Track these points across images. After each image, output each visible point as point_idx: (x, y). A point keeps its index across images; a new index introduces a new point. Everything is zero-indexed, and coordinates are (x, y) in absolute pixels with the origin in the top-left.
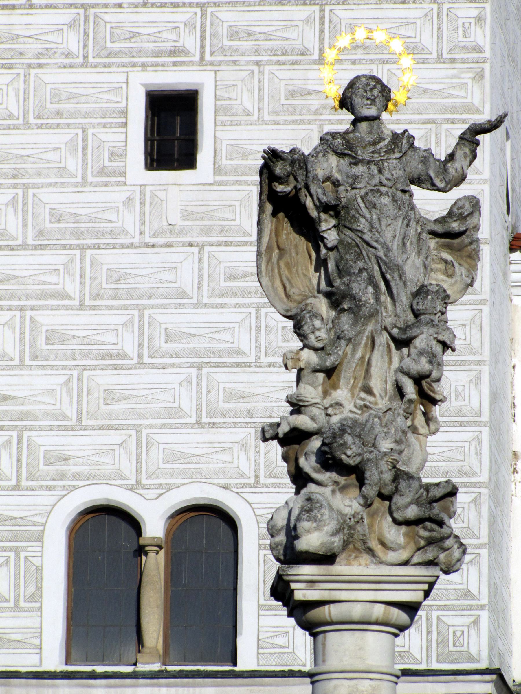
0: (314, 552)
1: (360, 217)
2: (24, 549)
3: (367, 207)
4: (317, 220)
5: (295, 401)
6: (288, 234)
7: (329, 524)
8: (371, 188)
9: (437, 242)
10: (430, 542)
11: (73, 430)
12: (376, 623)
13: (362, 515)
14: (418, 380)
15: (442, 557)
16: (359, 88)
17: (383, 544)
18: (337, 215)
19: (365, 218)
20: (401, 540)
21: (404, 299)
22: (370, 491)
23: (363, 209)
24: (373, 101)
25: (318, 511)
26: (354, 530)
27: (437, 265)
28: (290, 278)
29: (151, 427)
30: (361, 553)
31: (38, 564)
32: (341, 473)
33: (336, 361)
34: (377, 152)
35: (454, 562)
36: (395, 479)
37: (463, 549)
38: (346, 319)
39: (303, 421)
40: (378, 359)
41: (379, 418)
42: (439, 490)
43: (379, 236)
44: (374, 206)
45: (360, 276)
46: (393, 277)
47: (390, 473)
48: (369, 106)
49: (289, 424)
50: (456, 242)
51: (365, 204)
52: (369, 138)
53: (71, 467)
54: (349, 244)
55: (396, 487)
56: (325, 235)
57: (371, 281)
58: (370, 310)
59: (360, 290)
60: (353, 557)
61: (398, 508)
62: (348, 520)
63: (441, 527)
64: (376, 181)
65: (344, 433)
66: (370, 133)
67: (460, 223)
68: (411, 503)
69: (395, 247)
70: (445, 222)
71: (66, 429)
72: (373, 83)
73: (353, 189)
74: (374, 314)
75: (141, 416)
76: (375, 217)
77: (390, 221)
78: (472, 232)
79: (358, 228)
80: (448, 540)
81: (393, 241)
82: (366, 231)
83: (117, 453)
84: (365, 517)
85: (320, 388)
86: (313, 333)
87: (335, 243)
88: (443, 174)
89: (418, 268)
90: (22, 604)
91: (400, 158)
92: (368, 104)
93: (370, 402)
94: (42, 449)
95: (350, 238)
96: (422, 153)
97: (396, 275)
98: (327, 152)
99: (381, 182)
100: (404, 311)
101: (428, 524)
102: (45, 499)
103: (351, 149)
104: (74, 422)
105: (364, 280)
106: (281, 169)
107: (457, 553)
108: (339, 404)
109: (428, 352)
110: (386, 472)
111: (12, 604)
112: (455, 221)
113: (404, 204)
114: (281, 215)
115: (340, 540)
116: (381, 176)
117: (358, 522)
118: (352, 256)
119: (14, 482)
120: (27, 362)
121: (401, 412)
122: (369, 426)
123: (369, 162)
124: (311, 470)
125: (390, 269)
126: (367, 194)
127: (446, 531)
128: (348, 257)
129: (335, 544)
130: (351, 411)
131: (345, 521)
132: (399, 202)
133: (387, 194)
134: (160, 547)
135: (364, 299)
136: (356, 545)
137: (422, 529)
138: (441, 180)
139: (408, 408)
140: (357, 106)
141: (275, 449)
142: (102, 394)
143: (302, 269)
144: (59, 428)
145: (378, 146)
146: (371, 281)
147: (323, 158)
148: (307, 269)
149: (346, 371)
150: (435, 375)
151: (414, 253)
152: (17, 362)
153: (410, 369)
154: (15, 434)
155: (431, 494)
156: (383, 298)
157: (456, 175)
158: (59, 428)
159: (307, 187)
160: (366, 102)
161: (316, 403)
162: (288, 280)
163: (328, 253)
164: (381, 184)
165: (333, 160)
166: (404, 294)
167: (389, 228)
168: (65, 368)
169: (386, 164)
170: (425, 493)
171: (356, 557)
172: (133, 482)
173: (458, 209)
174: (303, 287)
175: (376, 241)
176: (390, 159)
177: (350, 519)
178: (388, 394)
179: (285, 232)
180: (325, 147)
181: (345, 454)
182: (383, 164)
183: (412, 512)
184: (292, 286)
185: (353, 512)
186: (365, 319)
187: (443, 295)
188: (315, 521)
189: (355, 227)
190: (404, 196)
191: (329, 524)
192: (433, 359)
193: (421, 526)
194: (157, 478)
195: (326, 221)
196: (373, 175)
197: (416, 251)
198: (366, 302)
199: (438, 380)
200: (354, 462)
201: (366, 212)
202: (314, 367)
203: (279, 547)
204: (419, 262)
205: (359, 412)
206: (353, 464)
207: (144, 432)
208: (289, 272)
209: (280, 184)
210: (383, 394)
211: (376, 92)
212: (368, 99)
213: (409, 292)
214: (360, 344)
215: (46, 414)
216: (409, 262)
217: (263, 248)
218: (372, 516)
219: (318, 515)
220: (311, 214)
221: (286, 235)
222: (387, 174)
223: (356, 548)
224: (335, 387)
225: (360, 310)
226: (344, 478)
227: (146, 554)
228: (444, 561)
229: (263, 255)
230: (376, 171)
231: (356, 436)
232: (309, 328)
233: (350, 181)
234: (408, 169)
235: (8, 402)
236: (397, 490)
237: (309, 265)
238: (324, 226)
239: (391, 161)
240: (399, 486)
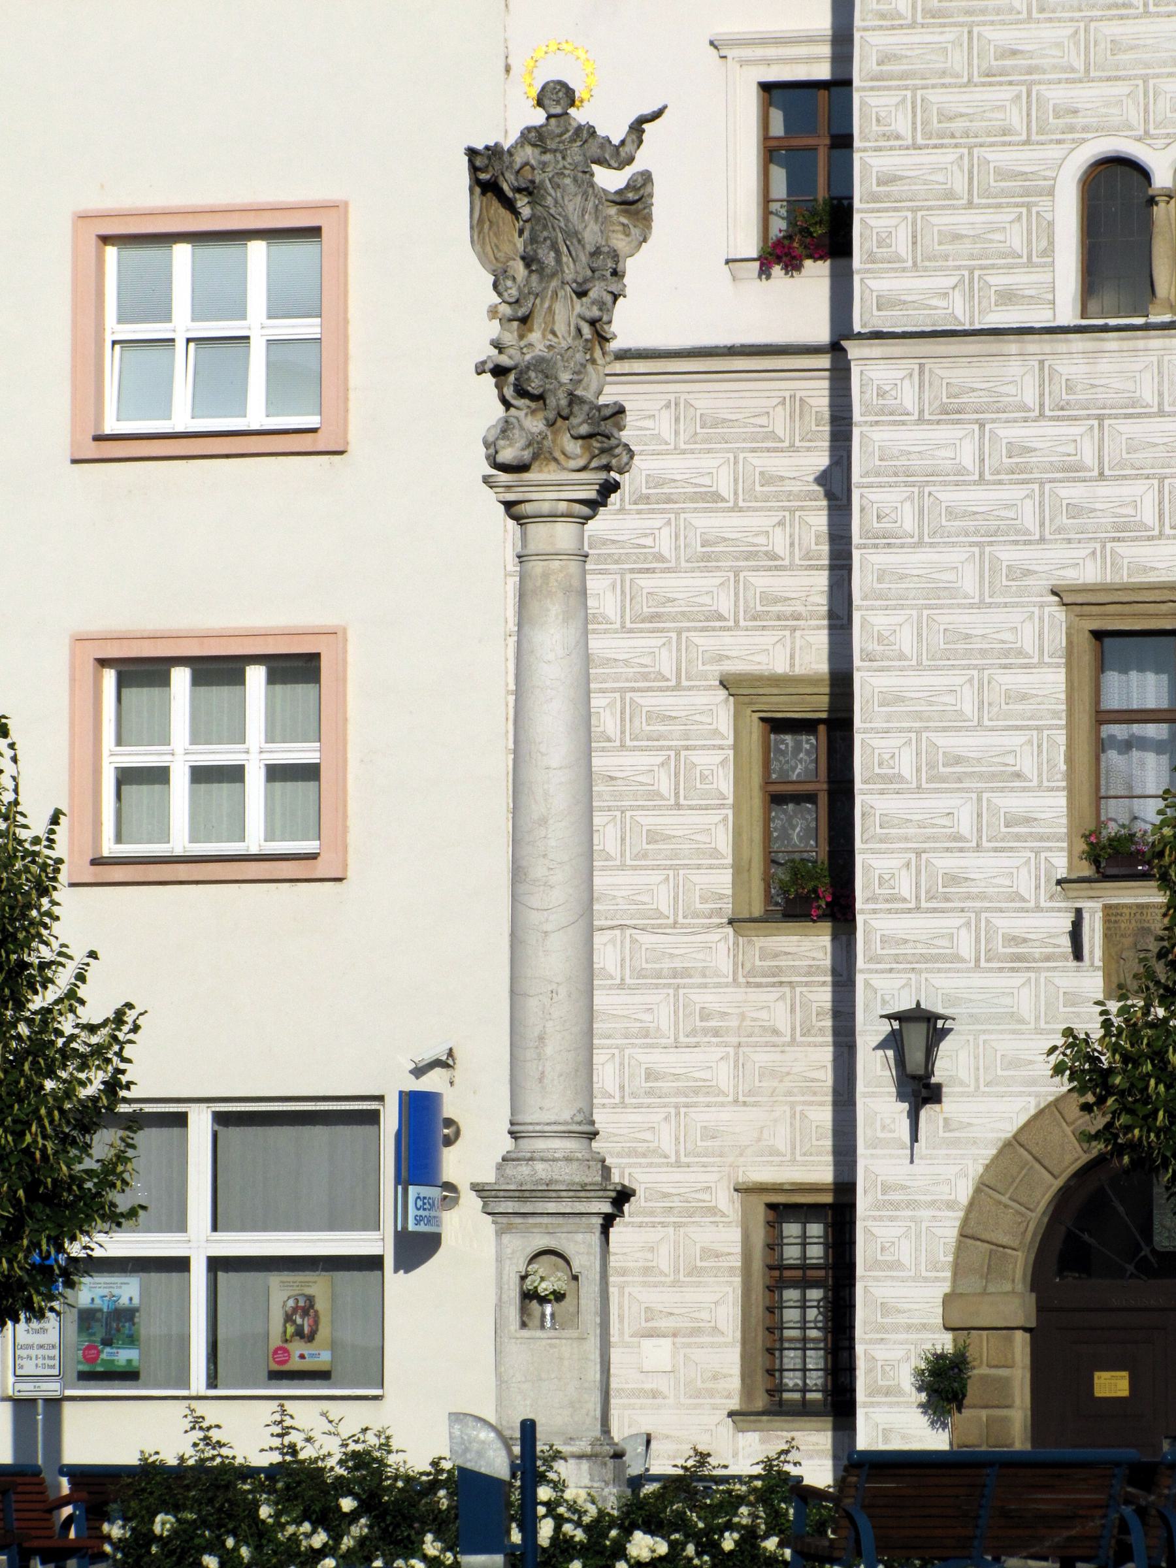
2: (1036, 204)
6: (496, 210)
10: (603, 451)
11: (1081, 82)
12: (562, 516)
14: (593, 323)
15: (614, 462)
17: (564, 454)
18: (530, 194)
20: (578, 451)
21: (584, 259)
22: (551, 415)
24: (558, 102)
29: (1157, 76)
31: (1050, 219)
36: (570, 404)
37: (631, 454)
38: (534, 277)
39: (504, 360)
40: (559, 307)
44: (559, 186)
50: (633, 207)
52: (558, 131)
53: (1080, 120)
57: (555, 247)
64: (560, 165)
71: (1073, 81)
74: (554, 275)
75: (1147, 66)
76: (559, 195)
83: (1125, 102)
88: (618, 156)
90: (1035, 259)
94: (1051, 102)
96: (601, 140)
97: (575, 241)
101: (599, 437)
102: (1054, 152)
104: (1081, 75)
107: (625, 458)
108: (530, 345)
111: (1025, 260)
119: (1024, 137)
120: (1035, 15)
123: (555, 151)
134: (1171, 197)
141: (488, 379)
142: (1109, 46)
144: (1068, 81)
146: (555, 247)
148: (513, 236)
150: (605, 319)
152: (1024, 15)
154: (1024, 89)
156: (564, 259)
158: (1068, 81)
159: (503, 174)
162: (497, 246)
164: (564, 167)
165: (529, 150)
168: (1072, 20)
172: (1141, 132)
183: (584, 429)
184: (499, 251)
192: (602, 305)
194: (1165, 127)
199: (610, 322)
201: (552, 191)
204: (596, 228)
207: (1151, 82)
210: (566, 335)
211: (561, 94)
215: (1054, 67)
216: (588, 229)
217: (475, 222)
218: (555, 433)
222: (569, 160)
224: (531, 330)
227: (1157, 204)
234: (588, 154)
235: (1018, 57)
236: (571, 413)
238: (519, 204)
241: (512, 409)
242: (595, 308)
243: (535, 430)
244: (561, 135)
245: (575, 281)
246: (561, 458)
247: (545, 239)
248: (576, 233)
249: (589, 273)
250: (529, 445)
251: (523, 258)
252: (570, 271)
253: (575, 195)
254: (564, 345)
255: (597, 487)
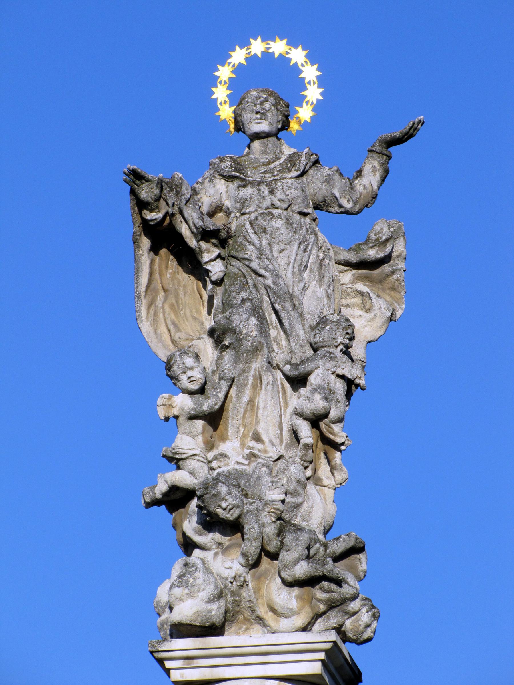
0: (188, 622)
1: (248, 244)
3: (255, 233)
4: (197, 250)
5: (170, 455)
7: (204, 589)
8: (262, 212)
9: (354, 275)
10: (332, 605)
13: (244, 577)
16: (248, 102)
17: (273, 610)
18: (223, 243)
19: (253, 244)
20: (294, 604)
21: (301, 333)
22: (252, 548)
23: (251, 235)
24: (263, 115)
25: (192, 575)
26: (239, 596)
27: (353, 300)
28: (177, 322)
30: (252, 624)
32: (224, 533)
33: (216, 404)
34: (270, 172)
35: (361, 628)
36: (280, 533)
38: (228, 356)
40: (266, 401)
41: (268, 467)
42: (339, 544)
43: (268, 263)
44: (264, 231)
45: (243, 307)
46: (283, 307)
47: (273, 526)
48: (259, 121)
49: (166, 482)
51: (254, 229)
52: (264, 159)
54: (235, 274)
55: (282, 542)
56: (208, 267)
57: (257, 311)
58: (252, 343)
59: (241, 322)
60: (243, 629)
61: (285, 566)
62: (230, 585)
63: (341, 586)
64: (267, 203)
65: (217, 483)
66: (264, 152)
67: (378, 250)
68: (298, 560)
69: (289, 275)
70: (360, 249)
72: (265, 96)
73: (243, 214)
74: (256, 350)
77: (283, 247)
78: (397, 262)
79: (245, 256)
80: (353, 602)
81: (287, 268)
82: (253, 258)
84: (249, 578)
85: (200, 438)
86: (185, 373)
87: (221, 275)
89: (320, 299)
91: (297, 177)
92: (257, 119)
93: (259, 450)
95: (237, 268)
97: (288, 305)
98: (214, 176)
99: (273, 204)
100: (301, 346)
101: (325, 584)
103: (239, 171)
105: (247, 310)
106: (146, 192)
108: (223, 455)
109: (324, 388)
110: (269, 524)
112: (372, 247)
113: (301, 227)
114: (164, 251)
115: (219, 608)
116: (273, 197)
117: (242, 586)
118: (237, 287)
121: (298, 460)
122: (255, 476)
123: (260, 183)
124: (193, 532)
125: (280, 298)
126: (256, 218)
127: (347, 591)
128: (232, 288)
129: (213, 613)
130: (237, 462)
131: (226, 586)
132: (294, 226)
133: (280, 216)
135: (245, 331)
136: (246, 615)
137: (320, 591)
138: (348, 201)
139: (305, 455)
140: (246, 123)
143: (191, 312)
145: (272, 166)
146: (257, 311)
147: (209, 184)
148: (199, 312)
149: (233, 418)
151: (314, 282)
153: (303, 409)
155: (329, 550)
156: (273, 333)
157: (365, 192)
159: (181, 212)
160: (255, 116)
161: (195, 455)
162: (174, 323)
163: (214, 288)
165: (221, 185)
166: (301, 327)
167: (282, 254)
169: (279, 184)
170: (322, 549)
171: (247, 629)
173: (375, 235)
174: (193, 331)
175: (265, 269)
176: (285, 178)
177: (232, 583)
178: (284, 442)
179: (171, 271)
180: (212, 172)
181: (220, 506)
182: (276, 184)
183: (302, 570)
184: (179, 330)
185: (233, 575)
186: (247, 354)
187: (344, 324)
188: (187, 587)
189: (241, 255)
190: (302, 220)
191: (204, 589)
193: (317, 587)
195: (208, 251)
196: (264, 197)
197: (316, 279)
198: (247, 334)
200: (232, 515)
201: (254, 238)
202: (189, 413)
203: (165, 626)
204: (321, 292)
205: (246, 462)
206: (231, 518)
208: (175, 315)
209: (151, 211)
210: (276, 441)
212: (257, 113)
213: (307, 325)
214: (246, 385)
216: (309, 292)
218: (258, 579)
219: (191, 579)
220: (190, 244)
221: (171, 274)
222: (279, 194)
223: (246, 619)
224: (224, 438)
225: (241, 345)
226: (228, 538)
228: (351, 627)
229: (143, 297)
230: (266, 192)
231: (234, 486)
232: (179, 367)
233: (238, 205)
237: (202, 307)
238: (206, 257)
239: (286, 180)
240: (284, 540)
241: (197, 552)
242: (318, 398)
243: (229, 574)
244: (269, 163)
245: (289, 363)
246: (269, 617)
247: (243, 301)
248: (291, 296)
249: (311, 352)
250: (220, 596)
251: (212, 333)
252: (283, 349)
253: (289, 243)
254: (273, 453)
255: (322, 656)
